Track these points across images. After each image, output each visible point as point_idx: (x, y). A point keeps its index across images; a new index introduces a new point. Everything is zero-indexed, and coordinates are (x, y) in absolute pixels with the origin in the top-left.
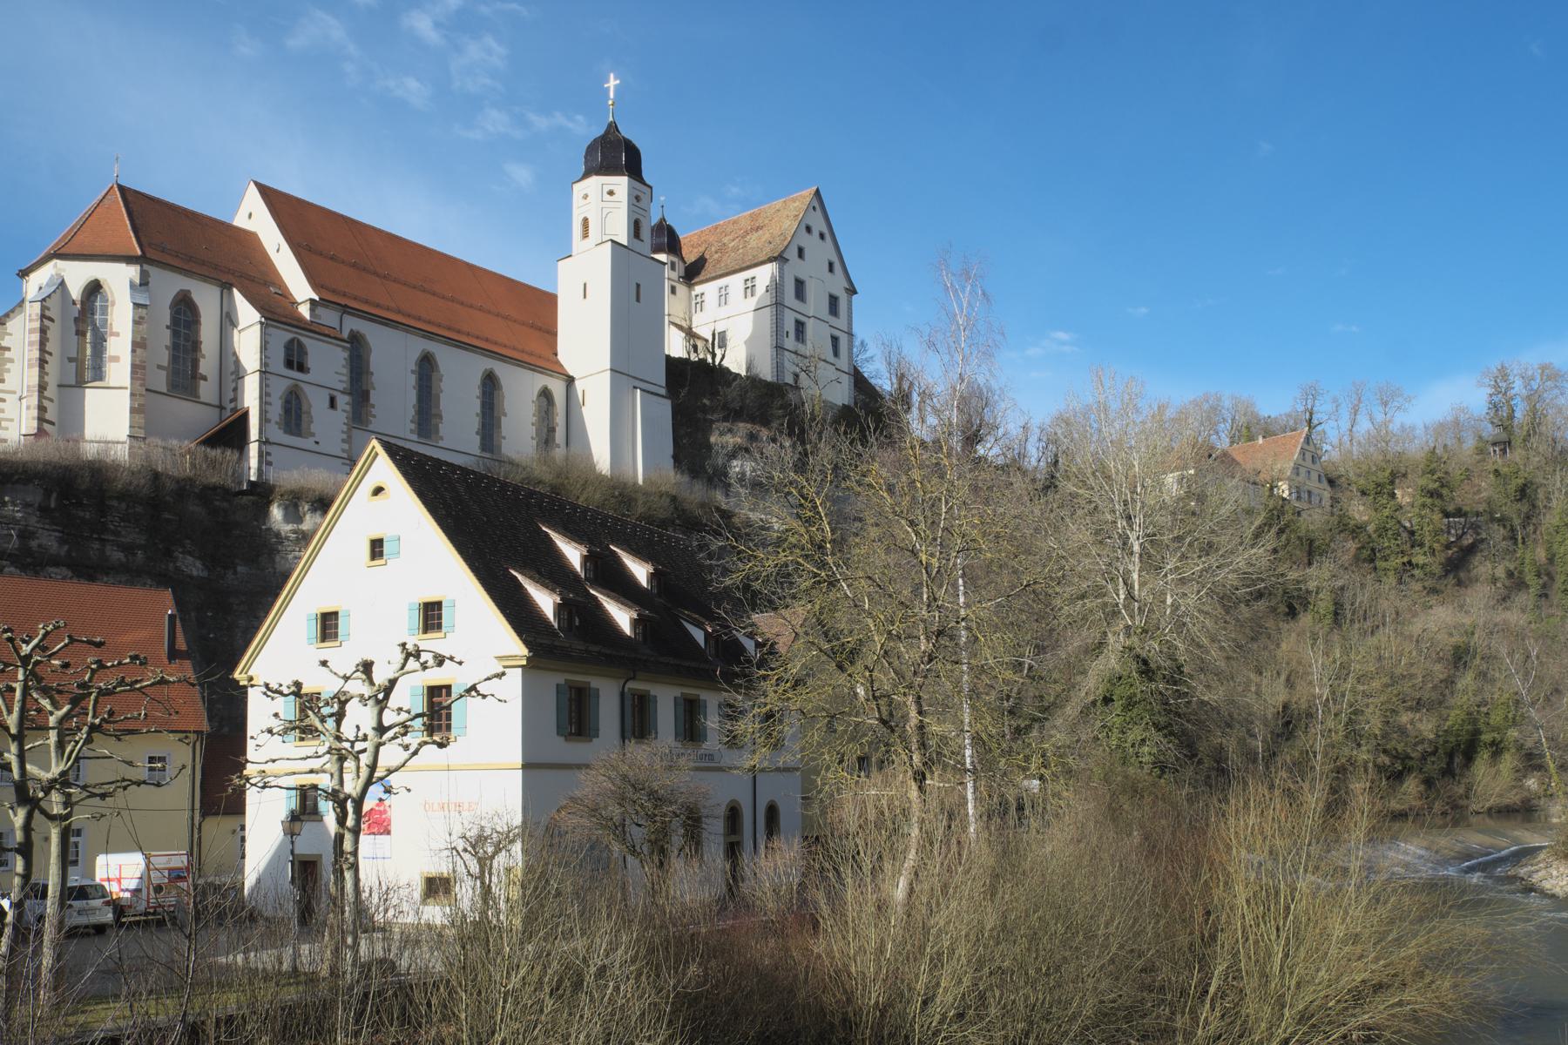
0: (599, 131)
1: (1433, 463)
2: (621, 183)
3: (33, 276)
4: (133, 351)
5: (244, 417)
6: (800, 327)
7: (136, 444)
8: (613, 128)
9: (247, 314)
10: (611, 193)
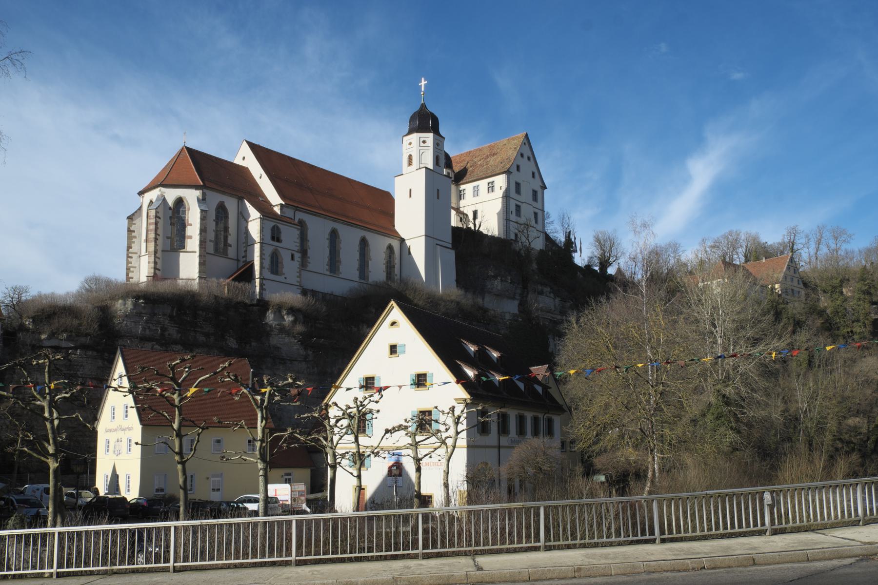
0: (417, 108)
1: (864, 275)
2: (429, 137)
3: (146, 195)
4: (201, 234)
5: (252, 266)
6: (518, 207)
7: (203, 281)
8: (423, 106)
9: (254, 214)
10: (424, 142)
